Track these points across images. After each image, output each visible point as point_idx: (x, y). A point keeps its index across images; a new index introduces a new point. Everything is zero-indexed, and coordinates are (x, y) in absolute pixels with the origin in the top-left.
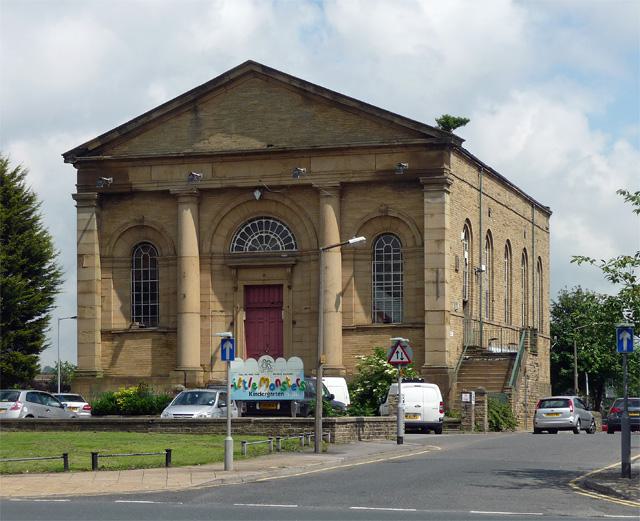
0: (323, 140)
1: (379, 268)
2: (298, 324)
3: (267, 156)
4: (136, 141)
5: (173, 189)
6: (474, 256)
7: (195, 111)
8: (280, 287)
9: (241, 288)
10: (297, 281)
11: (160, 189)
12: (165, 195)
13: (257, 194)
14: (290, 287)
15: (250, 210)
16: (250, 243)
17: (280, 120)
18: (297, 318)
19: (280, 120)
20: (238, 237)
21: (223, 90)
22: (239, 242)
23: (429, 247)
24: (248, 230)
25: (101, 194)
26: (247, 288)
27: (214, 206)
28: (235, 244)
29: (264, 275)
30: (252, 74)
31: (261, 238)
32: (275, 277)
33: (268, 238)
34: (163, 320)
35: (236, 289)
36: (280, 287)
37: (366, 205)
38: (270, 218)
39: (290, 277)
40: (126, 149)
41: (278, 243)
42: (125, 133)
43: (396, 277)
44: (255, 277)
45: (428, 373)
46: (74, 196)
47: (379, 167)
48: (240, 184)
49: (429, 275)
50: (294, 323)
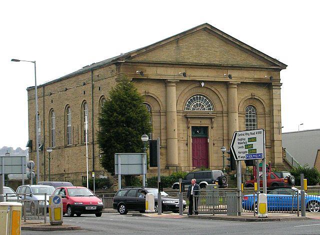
0: (231, 62)
1: (247, 121)
3: (172, 66)
6: (48, 169)
7: (177, 42)
9: (191, 128)
10: (215, 125)
17: (215, 51)
18: (215, 142)
19: (215, 51)
22: (188, 105)
23: (275, 113)
30: (208, 30)
32: (205, 123)
37: (247, 93)
39: (212, 123)
40: (145, 58)
42: (140, 52)
44: (197, 123)
47: (256, 77)
49: (275, 125)
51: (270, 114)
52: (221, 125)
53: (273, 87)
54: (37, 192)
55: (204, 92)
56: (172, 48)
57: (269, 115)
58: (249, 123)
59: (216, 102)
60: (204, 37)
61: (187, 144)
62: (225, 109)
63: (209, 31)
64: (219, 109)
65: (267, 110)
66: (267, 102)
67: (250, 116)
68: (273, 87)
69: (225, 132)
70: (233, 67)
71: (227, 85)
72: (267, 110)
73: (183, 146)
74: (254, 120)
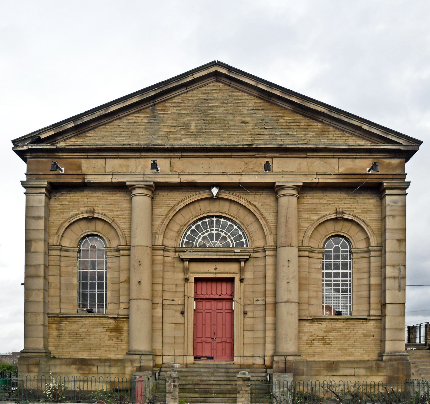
2: (249, 314)
3: (138, 154)
4: (91, 134)
5: (128, 180)
8: (231, 280)
9: (192, 280)
10: (248, 275)
11: (114, 180)
12: (122, 188)
13: (215, 191)
14: (242, 280)
15: (205, 208)
16: (200, 240)
18: (248, 309)
20: (189, 233)
21: (184, 90)
24: (198, 227)
25: (50, 183)
26: (197, 280)
27: (170, 200)
28: (185, 240)
29: (216, 269)
30: (219, 74)
31: (211, 236)
33: (218, 235)
34: (111, 309)
35: (187, 280)
36: (231, 280)
38: (221, 217)
39: (242, 270)
41: (229, 240)
43: (345, 275)
44: (207, 270)
45: (390, 360)
46: (25, 174)
48: (199, 179)
50: (245, 313)
51: (381, 251)
52: (261, 274)
53: (387, 192)
54: (411, 336)
55: (345, 230)
56: (140, 118)
57: (378, 253)
58: (333, 271)
59: (253, 227)
60: (215, 89)
61: (182, 313)
62: (271, 242)
63: (228, 81)
64: (259, 243)
65: (374, 242)
66: (374, 225)
67: (337, 257)
68: (387, 192)
69: (269, 287)
70: (284, 151)
71: (272, 189)
72: (374, 242)
73: (87, 320)
74: (345, 266)
